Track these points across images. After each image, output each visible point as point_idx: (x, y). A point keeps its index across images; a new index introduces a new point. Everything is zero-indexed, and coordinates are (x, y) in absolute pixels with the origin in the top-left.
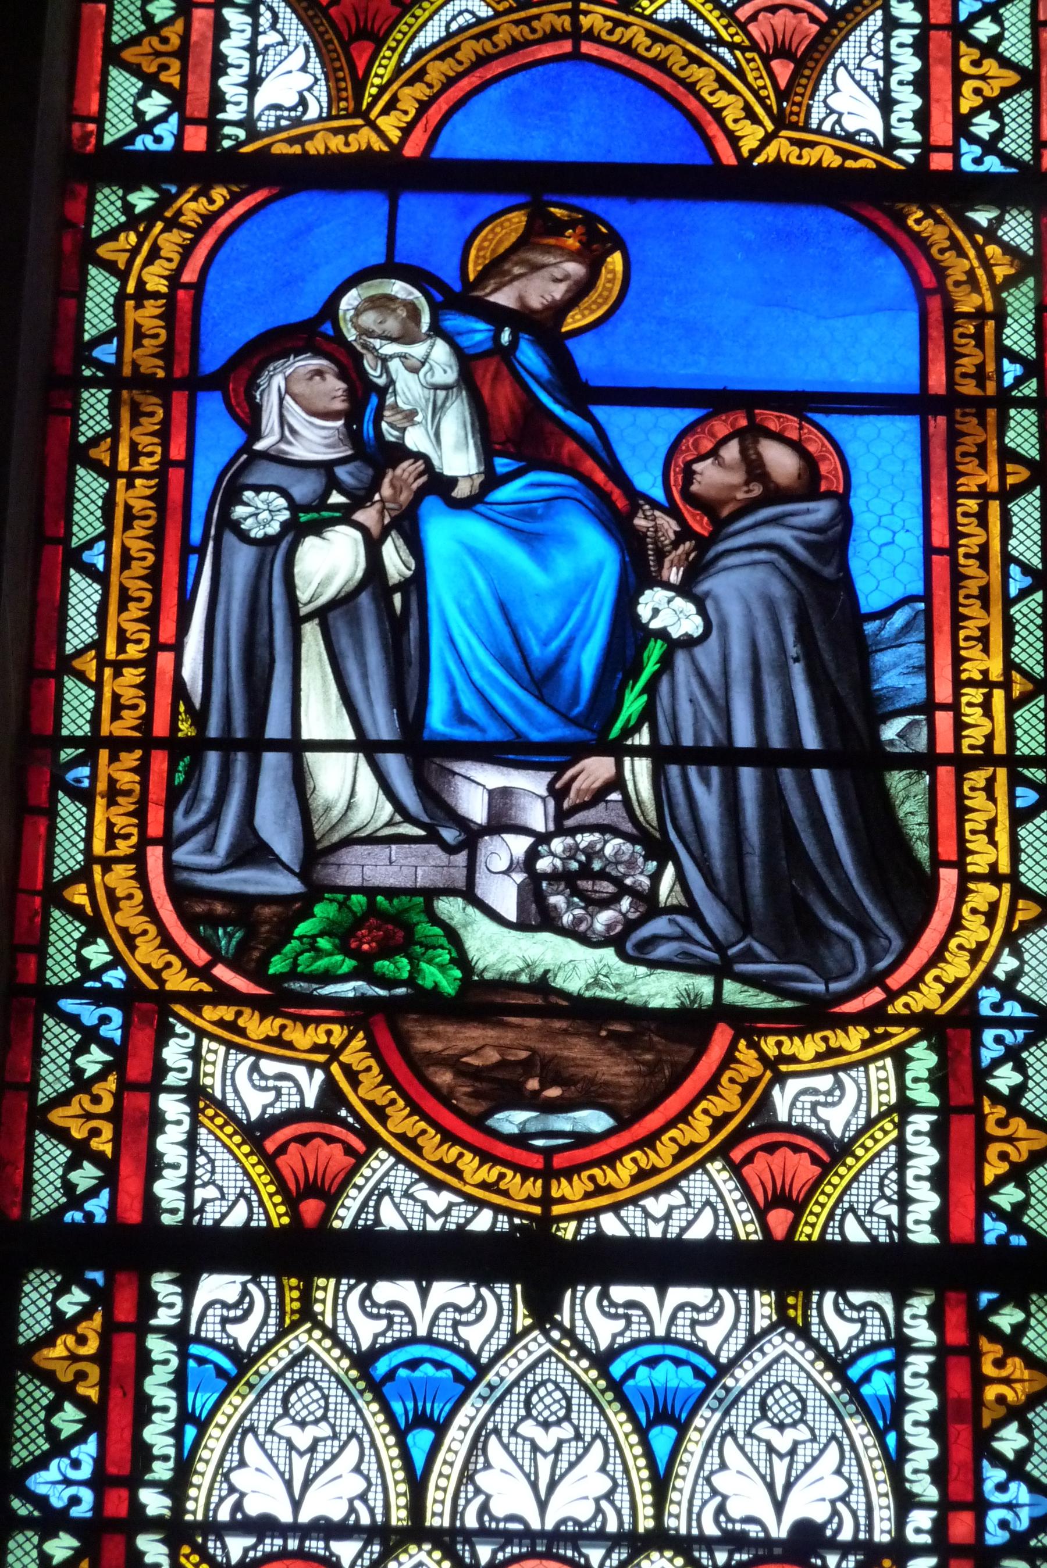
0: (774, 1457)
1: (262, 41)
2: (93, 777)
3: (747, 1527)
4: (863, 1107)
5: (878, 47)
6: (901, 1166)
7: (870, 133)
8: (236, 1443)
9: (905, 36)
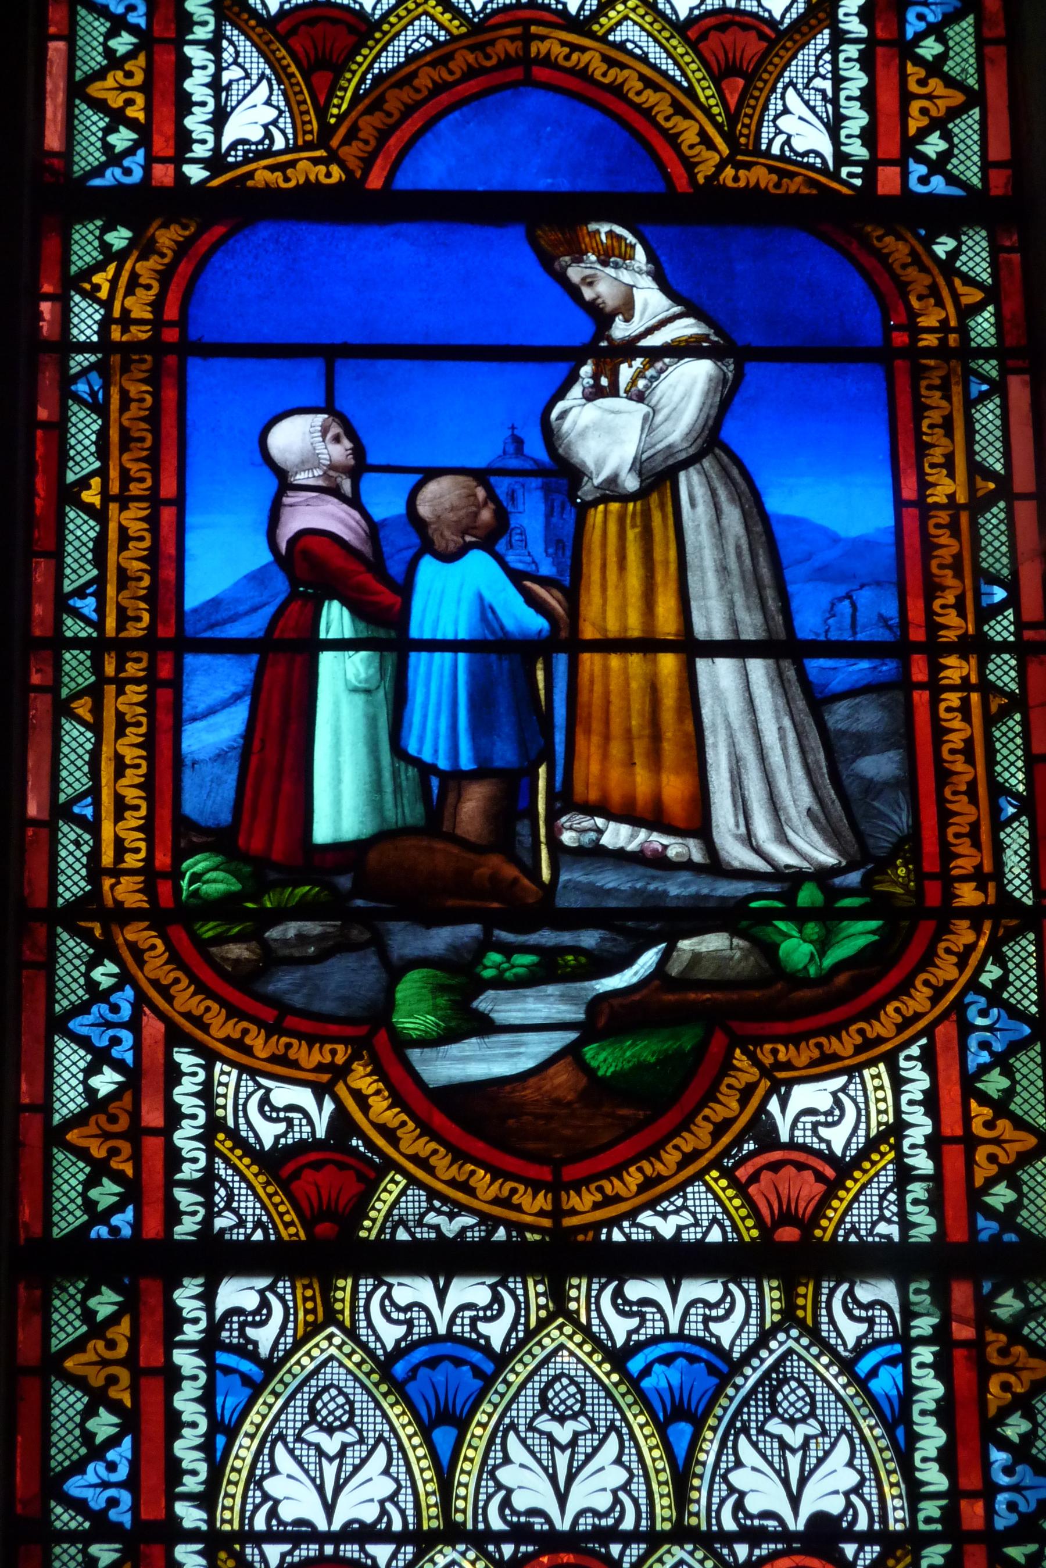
0: (788, 1454)
1: (226, 77)
3: (765, 1523)
4: (863, 1126)
5: (826, 69)
7: (818, 154)
8: (266, 1451)
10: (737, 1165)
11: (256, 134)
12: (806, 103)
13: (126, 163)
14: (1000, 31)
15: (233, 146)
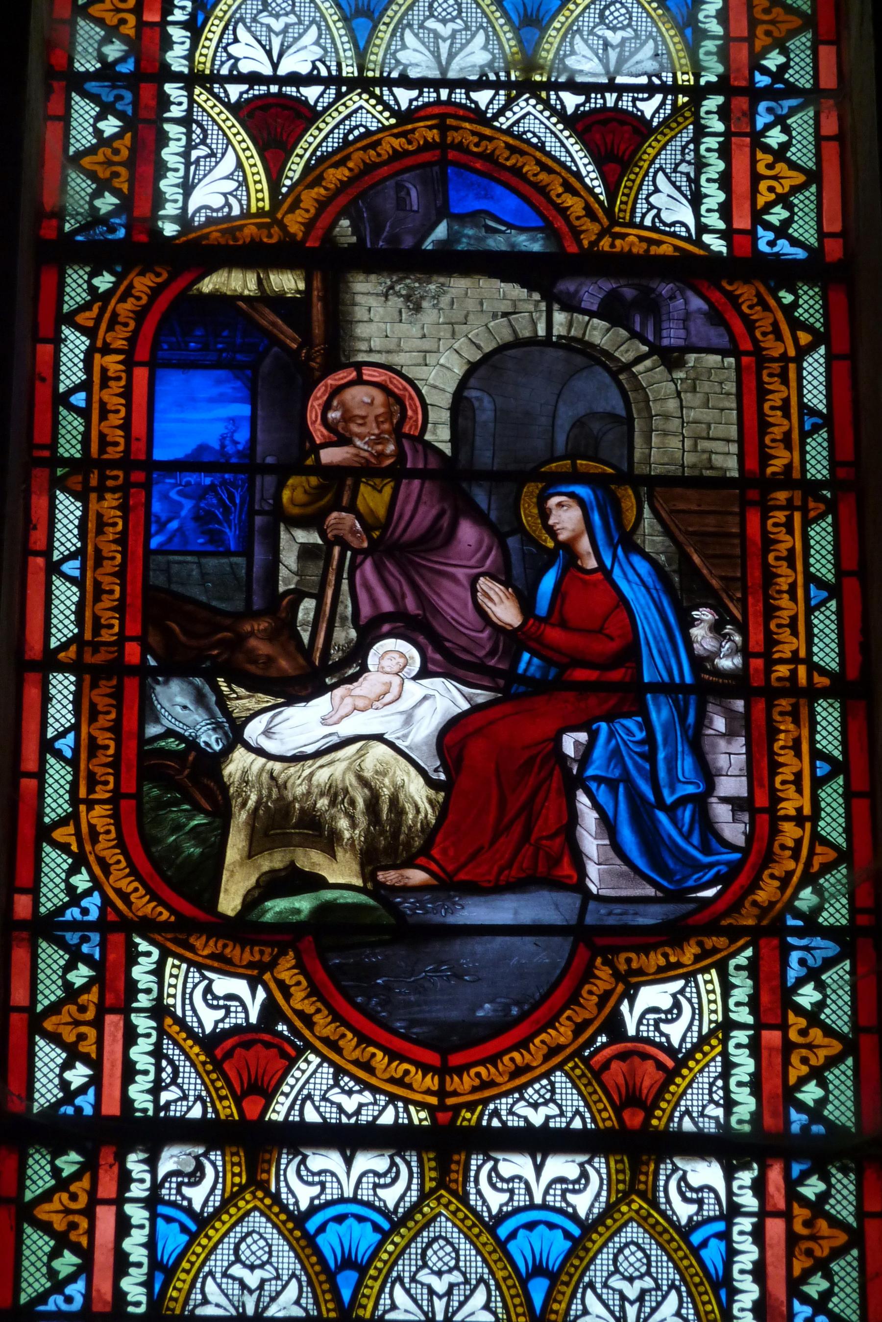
0: (627, 1304)
2: (89, 400)
6: (725, 1075)
9: (712, 142)
10: (593, 1055)
11: (217, 202)
12: (673, 184)
13: (73, 1188)
14: (837, 227)
15: (198, 210)
